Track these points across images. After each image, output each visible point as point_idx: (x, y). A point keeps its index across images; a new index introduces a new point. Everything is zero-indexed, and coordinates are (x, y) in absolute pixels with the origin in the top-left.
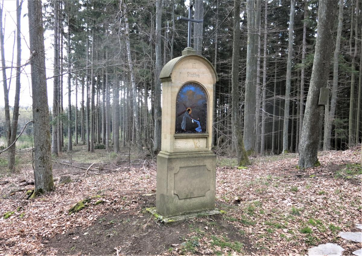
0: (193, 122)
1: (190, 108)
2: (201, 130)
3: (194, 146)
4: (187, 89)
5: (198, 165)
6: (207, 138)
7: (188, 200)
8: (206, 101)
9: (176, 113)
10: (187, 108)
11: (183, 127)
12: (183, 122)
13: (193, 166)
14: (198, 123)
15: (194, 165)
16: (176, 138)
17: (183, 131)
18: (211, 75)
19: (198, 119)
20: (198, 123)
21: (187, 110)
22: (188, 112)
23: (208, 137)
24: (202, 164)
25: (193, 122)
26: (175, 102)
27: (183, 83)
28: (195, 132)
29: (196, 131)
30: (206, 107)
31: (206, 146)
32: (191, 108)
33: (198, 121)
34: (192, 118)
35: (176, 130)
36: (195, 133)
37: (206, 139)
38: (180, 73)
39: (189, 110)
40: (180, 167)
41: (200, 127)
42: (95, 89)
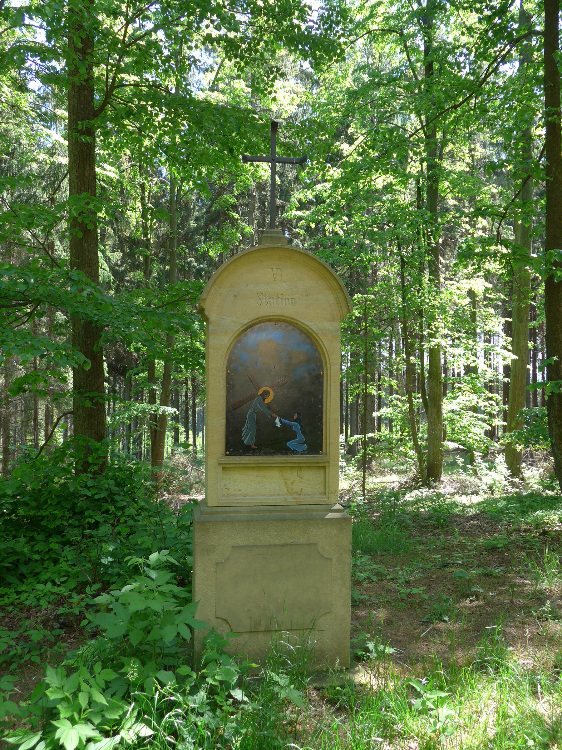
0: (278, 424)
1: (269, 389)
2: (305, 447)
3: (285, 490)
4: (253, 338)
5: (289, 541)
6: (325, 467)
7: (260, 636)
8: (321, 367)
9: (227, 401)
10: (258, 389)
11: (248, 439)
12: (247, 425)
13: (270, 546)
14: (296, 427)
15: (277, 542)
16: (225, 468)
17: (247, 450)
18: (331, 298)
19: (296, 416)
20: (296, 427)
21: (260, 392)
22: (264, 400)
23: (327, 465)
24: (303, 540)
25: (278, 424)
26: (225, 373)
27: (246, 321)
28: (287, 451)
29: (289, 449)
30: (322, 384)
31: (322, 490)
32: (271, 388)
33: (295, 421)
34: (274, 415)
35: (227, 447)
36: (286, 454)
37: (322, 472)
38: (235, 296)
39: (266, 393)
40: (233, 547)
41: (301, 437)
42: (246, 699)
